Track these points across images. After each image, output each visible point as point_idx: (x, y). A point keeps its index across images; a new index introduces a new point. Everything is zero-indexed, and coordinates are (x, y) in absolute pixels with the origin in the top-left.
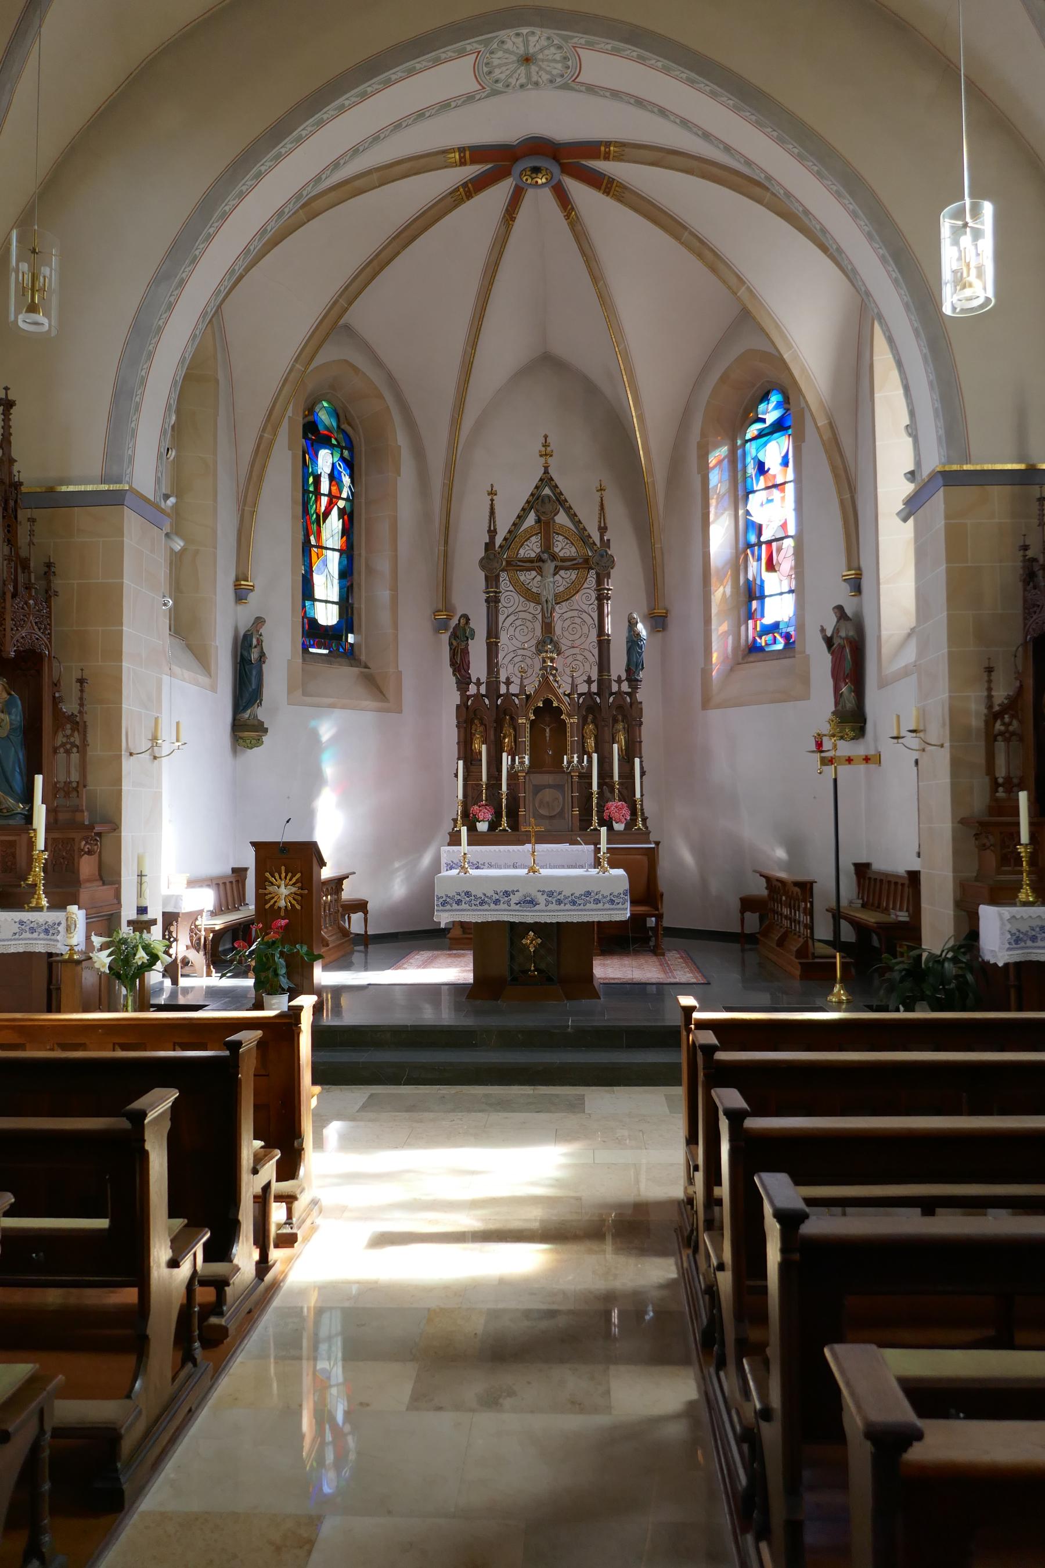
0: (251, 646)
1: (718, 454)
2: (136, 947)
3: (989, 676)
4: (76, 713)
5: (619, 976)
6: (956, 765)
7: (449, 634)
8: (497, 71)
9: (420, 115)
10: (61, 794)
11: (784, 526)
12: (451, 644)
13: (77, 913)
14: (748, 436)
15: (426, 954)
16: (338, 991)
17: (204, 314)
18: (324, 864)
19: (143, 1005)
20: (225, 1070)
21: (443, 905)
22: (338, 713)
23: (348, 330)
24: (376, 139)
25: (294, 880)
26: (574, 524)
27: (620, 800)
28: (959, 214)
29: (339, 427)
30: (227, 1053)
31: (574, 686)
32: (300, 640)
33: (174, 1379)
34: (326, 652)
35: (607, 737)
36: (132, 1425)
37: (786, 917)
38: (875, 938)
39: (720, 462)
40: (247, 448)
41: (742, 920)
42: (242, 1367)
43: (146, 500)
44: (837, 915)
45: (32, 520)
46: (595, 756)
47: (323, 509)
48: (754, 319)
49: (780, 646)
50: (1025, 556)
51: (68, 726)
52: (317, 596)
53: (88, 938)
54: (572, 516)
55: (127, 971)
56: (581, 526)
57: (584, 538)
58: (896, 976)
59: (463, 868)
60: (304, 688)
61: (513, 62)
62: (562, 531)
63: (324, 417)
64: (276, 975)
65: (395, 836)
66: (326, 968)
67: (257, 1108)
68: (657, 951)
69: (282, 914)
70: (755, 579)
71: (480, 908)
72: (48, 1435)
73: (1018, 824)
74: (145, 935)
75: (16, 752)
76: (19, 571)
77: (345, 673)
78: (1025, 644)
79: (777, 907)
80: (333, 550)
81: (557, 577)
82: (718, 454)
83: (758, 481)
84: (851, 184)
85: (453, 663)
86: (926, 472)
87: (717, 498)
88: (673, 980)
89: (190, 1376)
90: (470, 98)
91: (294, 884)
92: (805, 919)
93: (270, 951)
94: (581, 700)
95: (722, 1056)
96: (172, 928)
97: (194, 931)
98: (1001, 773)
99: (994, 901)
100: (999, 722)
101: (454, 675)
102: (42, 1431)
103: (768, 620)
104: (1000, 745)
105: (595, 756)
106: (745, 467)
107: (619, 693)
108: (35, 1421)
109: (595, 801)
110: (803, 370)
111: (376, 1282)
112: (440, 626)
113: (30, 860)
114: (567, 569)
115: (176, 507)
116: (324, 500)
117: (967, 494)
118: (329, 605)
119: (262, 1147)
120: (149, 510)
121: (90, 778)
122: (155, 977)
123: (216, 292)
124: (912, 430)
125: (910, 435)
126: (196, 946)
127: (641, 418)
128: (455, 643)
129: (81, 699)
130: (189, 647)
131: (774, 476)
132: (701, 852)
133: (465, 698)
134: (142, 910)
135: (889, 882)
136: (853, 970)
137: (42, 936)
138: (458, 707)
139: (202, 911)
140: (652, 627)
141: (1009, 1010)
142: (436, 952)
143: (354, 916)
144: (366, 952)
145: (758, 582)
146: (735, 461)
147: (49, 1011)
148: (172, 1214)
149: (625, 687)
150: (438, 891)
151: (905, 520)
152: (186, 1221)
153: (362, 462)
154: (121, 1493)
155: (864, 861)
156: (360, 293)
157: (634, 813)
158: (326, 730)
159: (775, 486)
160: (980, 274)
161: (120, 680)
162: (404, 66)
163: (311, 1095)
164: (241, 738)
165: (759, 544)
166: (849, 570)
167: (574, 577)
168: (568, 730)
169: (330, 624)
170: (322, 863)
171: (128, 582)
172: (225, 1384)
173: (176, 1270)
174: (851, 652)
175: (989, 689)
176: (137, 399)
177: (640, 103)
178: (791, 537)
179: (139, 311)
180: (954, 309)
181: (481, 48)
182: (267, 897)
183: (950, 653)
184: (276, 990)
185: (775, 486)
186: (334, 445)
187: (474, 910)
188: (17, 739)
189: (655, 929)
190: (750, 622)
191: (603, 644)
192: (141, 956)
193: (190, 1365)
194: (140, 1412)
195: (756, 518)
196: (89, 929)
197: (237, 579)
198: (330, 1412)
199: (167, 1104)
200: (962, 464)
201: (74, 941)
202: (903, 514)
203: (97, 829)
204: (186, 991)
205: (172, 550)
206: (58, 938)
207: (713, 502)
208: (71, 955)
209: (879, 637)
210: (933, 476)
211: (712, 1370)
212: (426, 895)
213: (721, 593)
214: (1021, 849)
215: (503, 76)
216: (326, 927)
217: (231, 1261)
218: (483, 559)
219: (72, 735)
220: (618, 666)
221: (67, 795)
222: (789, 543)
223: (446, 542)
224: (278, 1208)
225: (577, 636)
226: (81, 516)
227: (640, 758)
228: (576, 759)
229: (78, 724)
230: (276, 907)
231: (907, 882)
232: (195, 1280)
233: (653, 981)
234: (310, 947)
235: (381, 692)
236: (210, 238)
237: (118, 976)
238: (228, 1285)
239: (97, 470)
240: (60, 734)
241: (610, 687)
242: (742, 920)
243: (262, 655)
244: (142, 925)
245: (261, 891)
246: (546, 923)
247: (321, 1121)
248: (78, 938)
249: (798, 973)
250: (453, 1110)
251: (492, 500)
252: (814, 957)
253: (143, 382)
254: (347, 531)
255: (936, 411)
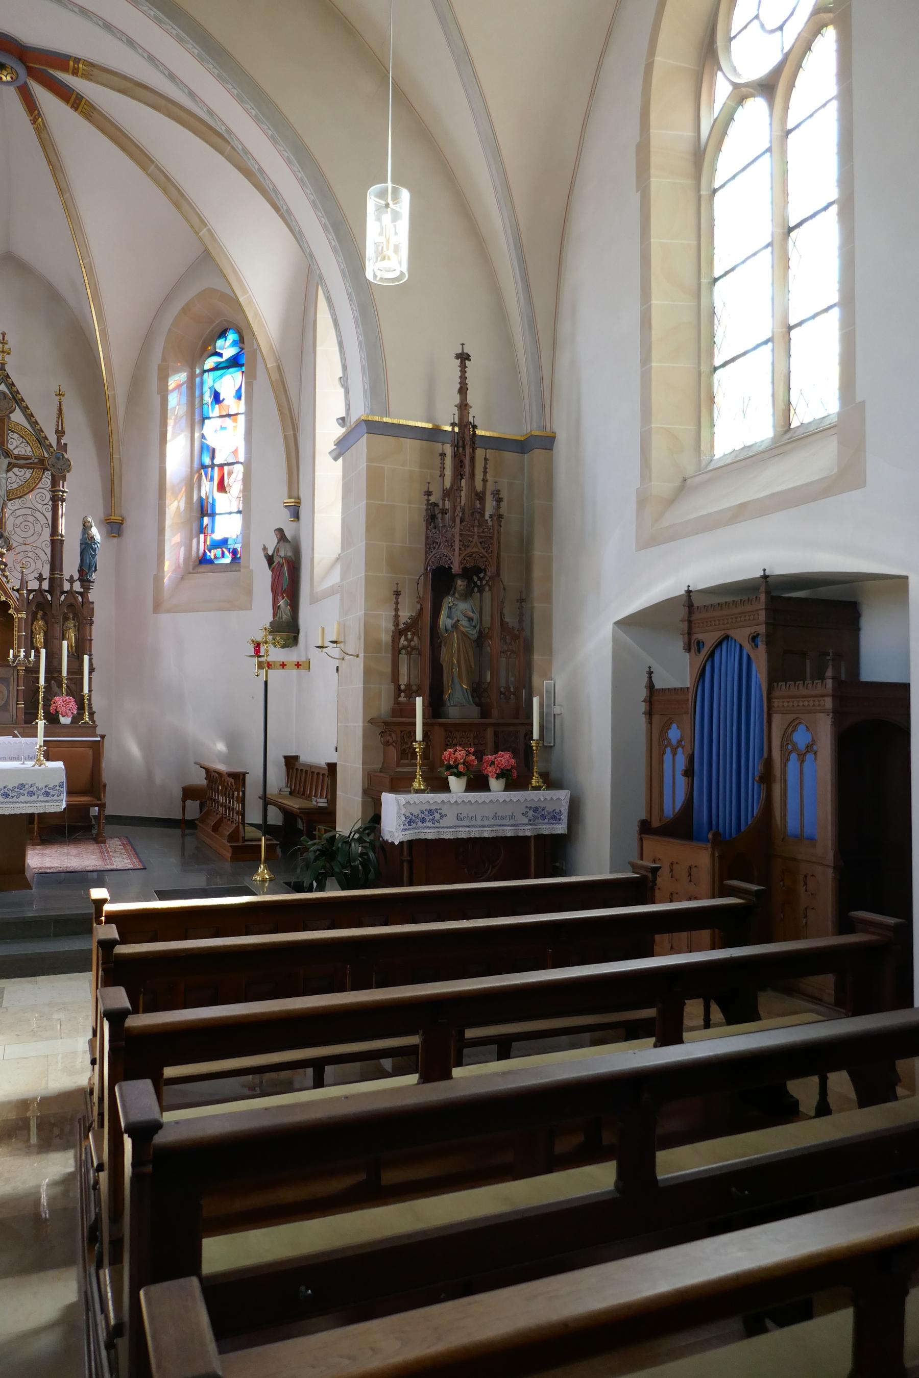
1: (177, 379)
3: (397, 598)
5: (55, 865)
6: (368, 672)
11: (235, 452)
14: (206, 367)
26: (29, 423)
27: (67, 695)
28: (382, 194)
31: (24, 583)
35: (58, 634)
37: (222, 805)
38: (299, 821)
39: (179, 387)
41: (184, 808)
44: (266, 801)
46: (43, 651)
48: (214, 260)
49: (228, 559)
50: (428, 500)
54: (29, 417)
56: (38, 427)
57: (41, 440)
58: (311, 856)
62: (18, 428)
68: (98, 840)
70: (207, 497)
73: (415, 724)
78: (425, 574)
79: (215, 796)
81: (10, 474)
82: (177, 379)
83: (213, 409)
84: (301, 155)
86: (354, 419)
87: (175, 419)
88: (109, 867)
92: (238, 806)
94: (31, 597)
95: (123, 949)
98: (403, 681)
99: (393, 789)
100: (403, 638)
103: (218, 536)
104: (403, 657)
105: (43, 651)
106: (202, 395)
107: (71, 592)
109: (41, 695)
110: (256, 314)
114: (21, 467)
117: (387, 442)
124: (344, 382)
125: (343, 386)
127: (103, 332)
131: (228, 407)
132: (148, 746)
135: (313, 773)
136: (279, 851)
140: (108, 533)
141: (402, 885)
145: (210, 500)
146: (193, 387)
149: (77, 587)
151: (336, 459)
155: (293, 754)
157: (81, 707)
159: (229, 416)
160: (396, 249)
165: (213, 466)
166: (290, 498)
167: (28, 475)
168: (16, 625)
174: (287, 572)
175: (397, 610)
177: (108, 27)
178: (241, 463)
180: (375, 276)
183: (367, 578)
185: (229, 416)
189: (97, 818)
190: (202, 536)
191: (56, 544)
195: (211, 442)
200: (382, 416)
202: (334, 454)
207: (171, 422)
209: (312, 559)
210: (359, 423)
211: (93, 1270)
213: (175, 506)
214: (416, 745)
220: (71, 565)
222: (239, 470)
225: (31, 533)
227: (90, 655)
228: (22, 654)
231: (326, 773)
233: (91, 868)
241: (62, 586)
242: (184, 808)
246: (10, 815)
249: (229, 855)
252: (245, 841)
255: (363, 368)
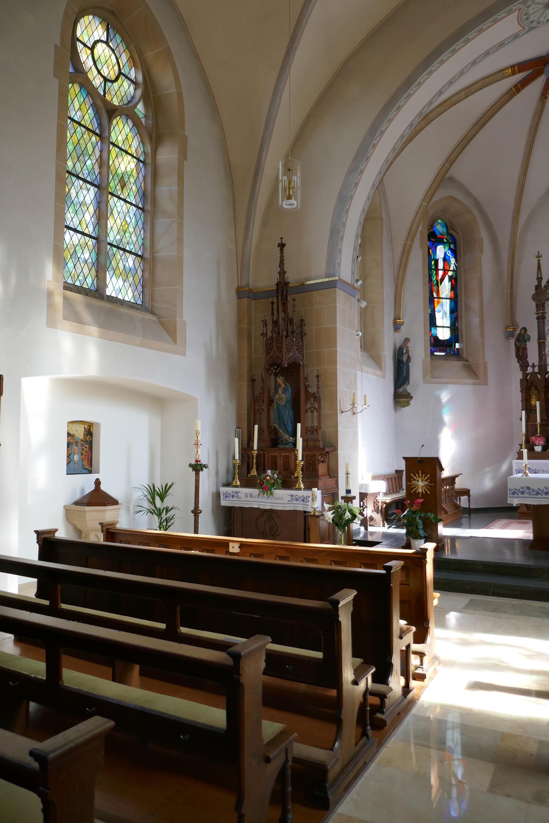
0: (402, 353)
2: (345, 510)
4: (315, 392)
7: (514, 339)
8: (532, 16)
9: (487, 54)
10: (309, 433)
12: (516, 345)
13: (317, 492)
15: (504, 521)
16: (454, 539)
17: (374, 185)
18: (443, 470)
19: (349, 541)
20: (385, 580)
21: (513, 493)
22: (451, 386)
23: (452, 179)
24: (462, 73)
25: (426, 478)
29: (447, 232)
30: (384, 572)
32: (429, 349)
33: (356, 745)
34: (443, 354)
36: (332, 767)
40: (399, 250)
42: (393, 745)
43: (347, 284)
45: (294, 300)
47: (440, 277)
51: (312, 399)
52: (438, 324)
53: (322, 504)
55: (341, 522)
59: (525, 473)
60: (432, 374)
61: (542, 9)
63: (440, 228)
64: (417, 529)
65: (485, 455)
66: (445, 526)
67: (402, 602)
69: (420, 496)
71: (536, 496)
72: (290, 763)
74: (350, 504)
75: (289, 413)
76: (289, 324)
77: (455, 365)
80: (446, 299)
85: (517, 356)
89: (365, 744)
90: (516, 36)
91: (426, 480)
93: (414, 516)
96: (364, 501)
97: (375, 503)
101: (518, 362)
102: (287, 760)
108: (283, 755)
111: (471, 710)
112: (509, 335)
113: (296, 465)
115: (363, 285)
116: (441, 273)
118: (444, 328)
119: (406, 625)
120: (349, 288)
121: (322, 425)
122: (356, 525)
123: (380, 172)
126: (377, 510)
128: (518, 344)
129: (318, 385)
130: (371, 356)
133: (525, 375)
134: (348, 491)
137: (301, 502)
138: (521, 380)
139: (380, 492)
142: (510, 520)
143: (462, 498)
144: (470, 518)
147: (305, 541)
148: (355, 655)
150: (510, 486)
152: (362, 660)
153: (461, 249)
154: (328, 800)
156: (457, 158)
158: (445, 396)
161: (336, 374)
162: (477, 29)
163: (435, 599)
164: (399, 402)
169: (445, 339)
170: (442, 469)
171: (339, 326)
172: (384, 752)
173: (356, 687)
176: (342, 234)
179: (341, 189)
181: (522, 6)
182: (412, 487)
184: (418, 537)
186: (445, 243)
187: (532, 498)
188: (289, 406)
192: (348, 515)
193: (365, 738)
194: (338, 759)
196: (323, 500)
197: (395, 319)
198: (453, 772)
199: (351, 598)
201: (316, 506)
203: (327, 450)
204: (372, 533)
205: (361, 308)
206: (309, 504)
208: (314, 513)
212: (502, 488)
215: (536, 18)
216: (446, 504)
217: (388, 685)
218: (534, 295)
219: (314, 403)
221: (312, 433)
223: (512, 288)
224: (416, 658)
226: (316, 295)
229: (316, 398)
230: (417, 492)
232: (367, 692)
234: (436, 515)
235: (475, 374)
236: (375, 146)
237: (337, 525)
238: (386, 698)
239: (323, 272)
240: (309, 403)
243: (409, 358)
244: (349, 499)
245: (409, 483)
247: (443, 611)
248: (317, 504)
250: (520, 614)
251: (539, 260)
253: (344, 224)
254: (454, 288)
